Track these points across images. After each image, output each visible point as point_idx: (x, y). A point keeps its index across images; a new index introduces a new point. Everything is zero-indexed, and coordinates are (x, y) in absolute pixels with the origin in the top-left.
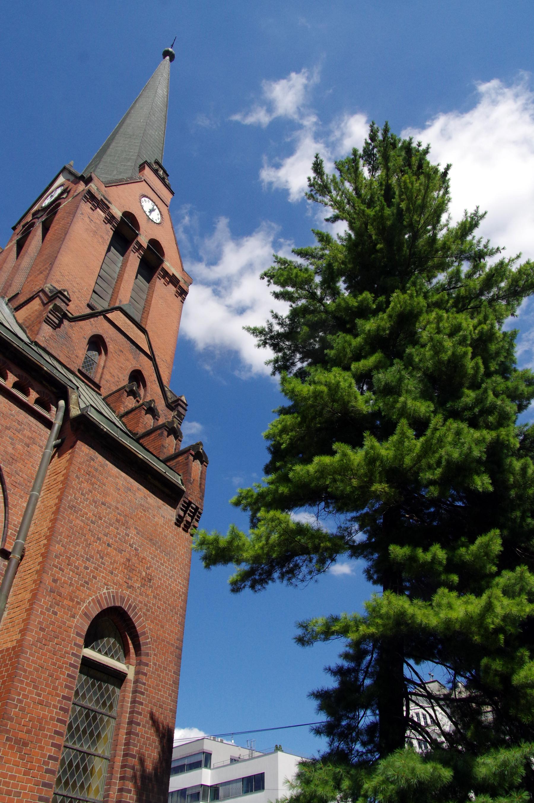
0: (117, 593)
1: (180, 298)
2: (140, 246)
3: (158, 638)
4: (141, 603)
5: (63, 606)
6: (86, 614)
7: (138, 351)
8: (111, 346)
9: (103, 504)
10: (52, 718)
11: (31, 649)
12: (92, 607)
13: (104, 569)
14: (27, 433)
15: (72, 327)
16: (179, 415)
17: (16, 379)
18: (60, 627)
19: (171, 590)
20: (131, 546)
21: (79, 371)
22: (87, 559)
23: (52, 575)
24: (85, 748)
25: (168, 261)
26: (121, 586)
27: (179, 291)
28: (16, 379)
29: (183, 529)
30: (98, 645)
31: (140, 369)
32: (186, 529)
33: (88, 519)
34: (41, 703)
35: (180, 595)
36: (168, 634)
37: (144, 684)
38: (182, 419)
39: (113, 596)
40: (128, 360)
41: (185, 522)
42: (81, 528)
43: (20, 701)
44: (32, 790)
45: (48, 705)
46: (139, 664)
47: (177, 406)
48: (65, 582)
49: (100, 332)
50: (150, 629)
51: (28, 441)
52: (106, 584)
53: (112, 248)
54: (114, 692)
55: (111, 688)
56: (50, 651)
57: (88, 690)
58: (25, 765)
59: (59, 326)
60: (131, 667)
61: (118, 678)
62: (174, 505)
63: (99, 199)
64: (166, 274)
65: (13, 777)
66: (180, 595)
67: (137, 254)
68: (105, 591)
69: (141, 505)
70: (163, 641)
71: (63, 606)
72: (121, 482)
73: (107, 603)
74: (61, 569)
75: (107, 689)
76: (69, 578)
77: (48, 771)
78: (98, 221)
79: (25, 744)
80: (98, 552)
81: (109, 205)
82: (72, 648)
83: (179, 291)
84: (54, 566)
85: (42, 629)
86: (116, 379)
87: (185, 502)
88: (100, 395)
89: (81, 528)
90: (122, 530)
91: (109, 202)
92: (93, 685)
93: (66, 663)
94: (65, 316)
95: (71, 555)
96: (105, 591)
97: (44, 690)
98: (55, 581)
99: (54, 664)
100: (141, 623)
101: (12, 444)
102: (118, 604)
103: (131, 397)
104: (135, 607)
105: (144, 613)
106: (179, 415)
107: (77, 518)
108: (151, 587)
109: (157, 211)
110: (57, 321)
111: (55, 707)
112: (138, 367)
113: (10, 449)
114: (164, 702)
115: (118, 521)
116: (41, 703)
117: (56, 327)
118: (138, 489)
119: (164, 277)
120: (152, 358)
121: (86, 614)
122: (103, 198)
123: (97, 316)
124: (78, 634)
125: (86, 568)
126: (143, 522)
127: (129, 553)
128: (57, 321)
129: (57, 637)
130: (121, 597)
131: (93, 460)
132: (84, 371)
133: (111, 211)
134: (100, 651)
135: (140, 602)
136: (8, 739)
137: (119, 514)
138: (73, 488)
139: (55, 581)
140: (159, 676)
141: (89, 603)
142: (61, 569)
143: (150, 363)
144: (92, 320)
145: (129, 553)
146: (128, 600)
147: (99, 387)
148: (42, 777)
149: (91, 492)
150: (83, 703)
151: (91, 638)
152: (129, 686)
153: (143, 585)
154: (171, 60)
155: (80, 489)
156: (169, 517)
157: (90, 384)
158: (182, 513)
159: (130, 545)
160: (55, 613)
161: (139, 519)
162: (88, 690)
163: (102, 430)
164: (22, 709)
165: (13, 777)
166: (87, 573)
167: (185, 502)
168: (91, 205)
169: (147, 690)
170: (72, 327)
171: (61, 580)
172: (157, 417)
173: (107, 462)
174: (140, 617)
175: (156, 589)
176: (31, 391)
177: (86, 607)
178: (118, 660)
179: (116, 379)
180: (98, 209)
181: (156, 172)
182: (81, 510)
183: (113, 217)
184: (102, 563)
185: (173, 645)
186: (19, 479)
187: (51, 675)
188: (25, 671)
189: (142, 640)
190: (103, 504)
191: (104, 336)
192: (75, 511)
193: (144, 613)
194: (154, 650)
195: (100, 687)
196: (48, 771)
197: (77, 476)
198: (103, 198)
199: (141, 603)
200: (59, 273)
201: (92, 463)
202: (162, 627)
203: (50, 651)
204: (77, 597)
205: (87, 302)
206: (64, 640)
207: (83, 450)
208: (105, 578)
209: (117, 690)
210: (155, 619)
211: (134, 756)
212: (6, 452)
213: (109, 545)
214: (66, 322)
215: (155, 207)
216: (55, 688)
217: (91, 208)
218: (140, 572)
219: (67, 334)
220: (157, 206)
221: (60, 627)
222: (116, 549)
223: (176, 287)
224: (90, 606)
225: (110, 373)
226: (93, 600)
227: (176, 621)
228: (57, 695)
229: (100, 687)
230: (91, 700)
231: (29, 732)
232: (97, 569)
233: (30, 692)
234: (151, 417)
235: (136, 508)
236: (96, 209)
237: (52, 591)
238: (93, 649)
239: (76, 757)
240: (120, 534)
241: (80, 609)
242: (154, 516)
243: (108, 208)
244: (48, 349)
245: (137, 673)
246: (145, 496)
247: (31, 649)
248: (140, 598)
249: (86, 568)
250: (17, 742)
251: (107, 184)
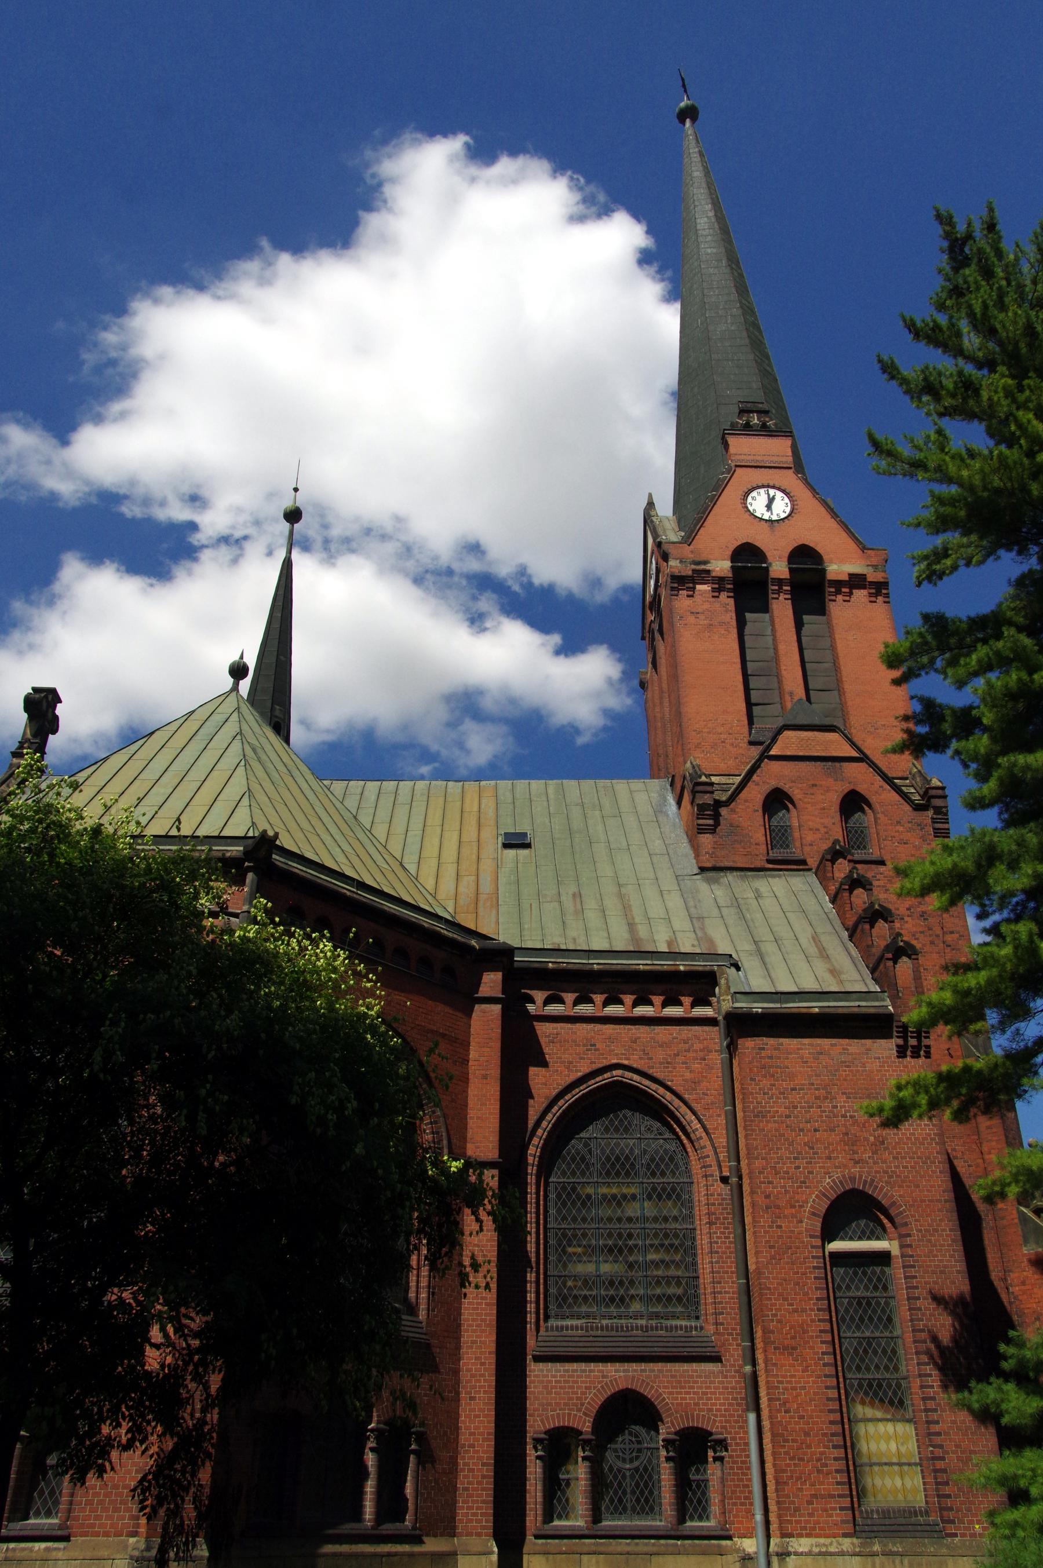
0: (844, 1176)
1: (880, 599)
2: (780, 582)
3: (915, 1201)
4: (879, 1172)
5: (785, 1217)
6: (814, 1214)
7: (837, 764)
8: (796, 791)
9: (792, 1089)
10: (812, 1321)
11: (767, 1268)
12: (819, 1204)
13: (819, 1158)
14: (697, 1046)
15: (733, 811)
16: (938, 810)
17: (662, 998)
18: (791, 1237)
19: (916, 1139)
20: (844, 1116)
21: (769, 861)
22: (795, 1158)
23: (762, 1193)
24: (867, 1334)
25: (831, 562)
26: (845, 1166)
27: (873, 591)
28: (662, 998)
29: (912, 1057)
30: (847, 1233)
31: (852, 787)
32: (916, 1055)
33: (781, 1116)
34: (795, 1311)
35: (932, 1139)
36: (928, 1191)
37: (912, 1256)
38: (946, 814)
39: (841, 1182)
40: (828, 791)
41: (910, 1049)
42: (776, 1130)
43: (775, 1315)
44: (814, 1382)
45: (804, 1310)
46: (901, 1237)
47: (929, 800)
48: (779, 1193)
49: (773, 784)
50: (900, 1196)
51: (701, 1054)
52: (825, 1173)
53: (748, 615)
54: (883, 1272)
55: (878, 1270)
56: (787, 1263)
57: (852, 1280)
58: (801, 1365)
59: (717, 824)
60: (892, 1242)
61: (883, 1258)
62: (888, 1036)
63: (690, 573)
64: (838, 584)
65: (792, 1376)
66: (932, 1139)
67: (782, 596)
68: (828, 1180)
69: (842, 1062)
70: (922, 1201)
71: (785, 1217)
72: (805, 1053)
73: (835, 1192)
74: (770, 1183)
75: (874, 1273)
76: (782, 1187)
77: (825, 1365)
78: (706, 606)
79: (794, 1348)
80: (805, 1144)
81: (708, 567)
82: (809, 1252)
83: (873, 591)
84: (761, 1182)
85: (771, 1247)
86: (823, 830)
87: (897, 1027)
88: (810, 870)
89: (776, 1130)
90: (827, 1105)
91: (705, 563)
92: (855, 1274)
93: (809, 1267)
94: (718, 804)
95: (775, 1163)
96: (828, 1180)
97: (795, 1299)
98: (767, 1197)
99: (798, 1273)
100: (884, 1193)
101: (687, 1068)
102: (849, 1186)
103: (840, 860)
104: (872, 1181)
105: (886, 1182)
106: (938, 810)
107: (767, 1122)
108: (886, 1149)
109: (779, 495)
110: (711, 822)
111: (812, 1310)
112: (846, 788)
113: (688, 1075)
114: (945, 1267)
115: (817, 1098)
116: (795, 1311)
117: (713, 830)
118: (832, 1045)
119: (838, 592)
120: (863, 758)
121: (814, 1214)
122: (693, 567)
123: (759, 766)
124: (811, 1236)
125: (798, 1167)
126: (852, 1080)
127: (845, 1125)
128: (711, 822)
129: (790, 1248)
130: (850, 1178)
131: (763, 1049)
132: (774, 854)
133: (714, 574)
134: (851, 1239)
135: (876, 1172)
136: (775, 1348)
137: (816, 1089)
138: (752, 1093)
139: (767, 1197)
140: (930, 1241)
141: (814, 1201)
142: (770, 1183)
143: (863, 765)
144: (755, 777)
145: (845, 1125)
146: (861, 1177)
147: (803, 862)
148: (820, 1370)
149: (774, 1085)
150: (851, 1294)
151: (829, 1233)
152: (897, 1263)
153: (875, 1152)
154: (694, 120)
155: (760, 1089)
156: (887, 1053)
157: (789, 867)
158: (900, 1042)
159: (843, 1116)
160: (780, 1227)
161: (845, 1080)
162: (852, 1280)
163: (757, 1013)
164: (779, 1321)
165: (792, 1376)
166: (800, 1173)
167: (897, 1027)
168: (685, 593)
169: (918, 1261)
170: (733, 811)
171: (773, 1192)
172: (868, 887)
173: (781, 1040)
174: (882, 1188)
175: (895, 1148)
176: (682, 998)
177: (812, 1207)
178: (878, 1239)
179: (823, 830)
180: (699, 587)
181: (747, 429)
182: (769, 1112)
183: (721, 580)
184: (814, 1153)
185: (938, 1201)
186: (709, 1099)
187: (798, 1284)
188: (769, 1289)
189: (893, 1212)
190: (792, 1089)
191: (781, 785)
192: (763, 1117)
193: (886, 1182)
194: (913, 1216)
195: (865, 1273)
196: (825, 1365)
197: (752, 1079)
198: (693, 567)
199: (879, 1172)
200: (694, 733)
201: (763, 1053)
202: (917, 1186)
203: (787, 1263)
204: (798, 1201)
205: (746, 740)
206: (798, 1248)
207: (748, 1045)
208: (823, 1167)
209: (886, 1269)
210: (903, 1182)
211: (923, 1331)
212: (686, 1080)
213: (816, 1130)
214: (724, 811)
215: (772, 492)
216: (807, 1294)
217: (688, 596)
218: (866, 1139)
219: (731, 825)
220: (773, 487)
221: (791, 1237)
222: (826, 1130)
223: (865, 588)
224: (814, 1204)
225: (811, 829)
226: (817, 1196)
227: (934, 1172)
228: (810, 1299)
229: (865, 1273)
230: (858, 1289)
231: (794, 1338)
232: (811, 1163)
233: (780, 1305)
234: (861, 890)
235: (836, 1071)
236: (694, 588)
237: (767, 1207)
238: (842, 1239)
239: (860, 1344)
240: (825, 1111)
241: (805, 1211)
242: (864, 1065)
243: (708, 572)
244: (718, 865)
245: (902, 1246)
246: (844, 1049)
247: (767, 1268)
248: (876, 1168)
249: (798, 1167)
250: (785, 1348)
251: (689, 538)
